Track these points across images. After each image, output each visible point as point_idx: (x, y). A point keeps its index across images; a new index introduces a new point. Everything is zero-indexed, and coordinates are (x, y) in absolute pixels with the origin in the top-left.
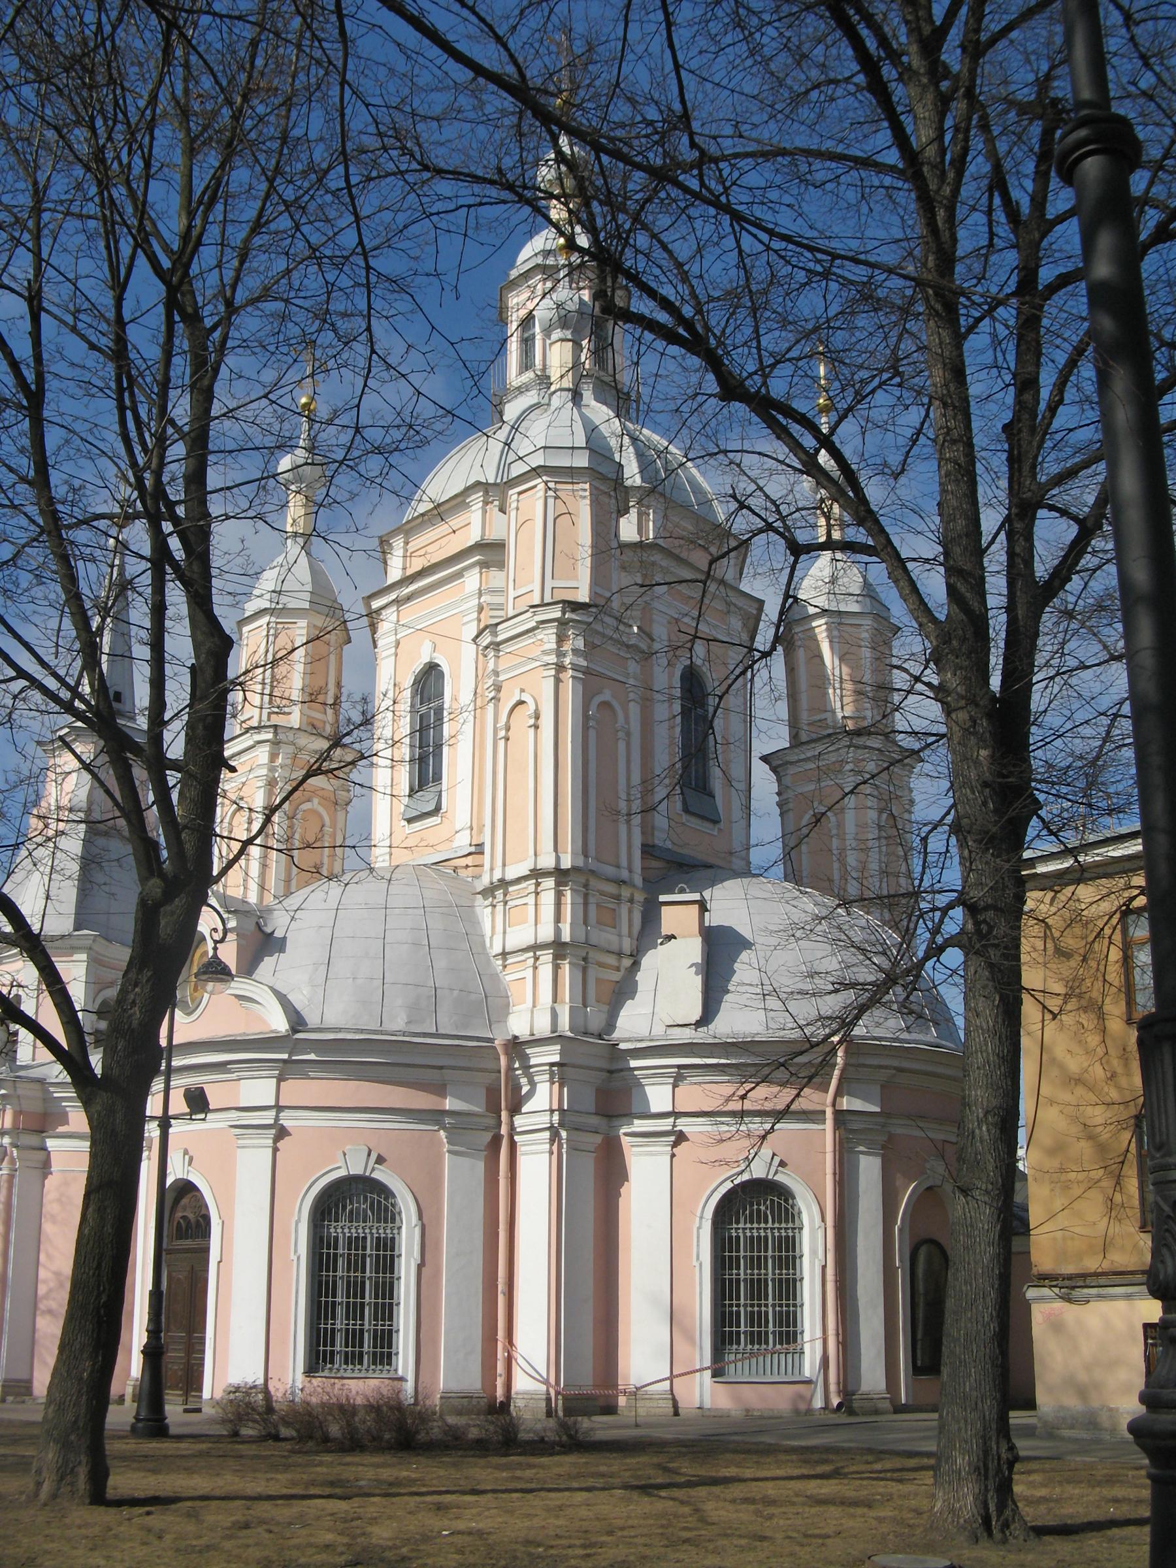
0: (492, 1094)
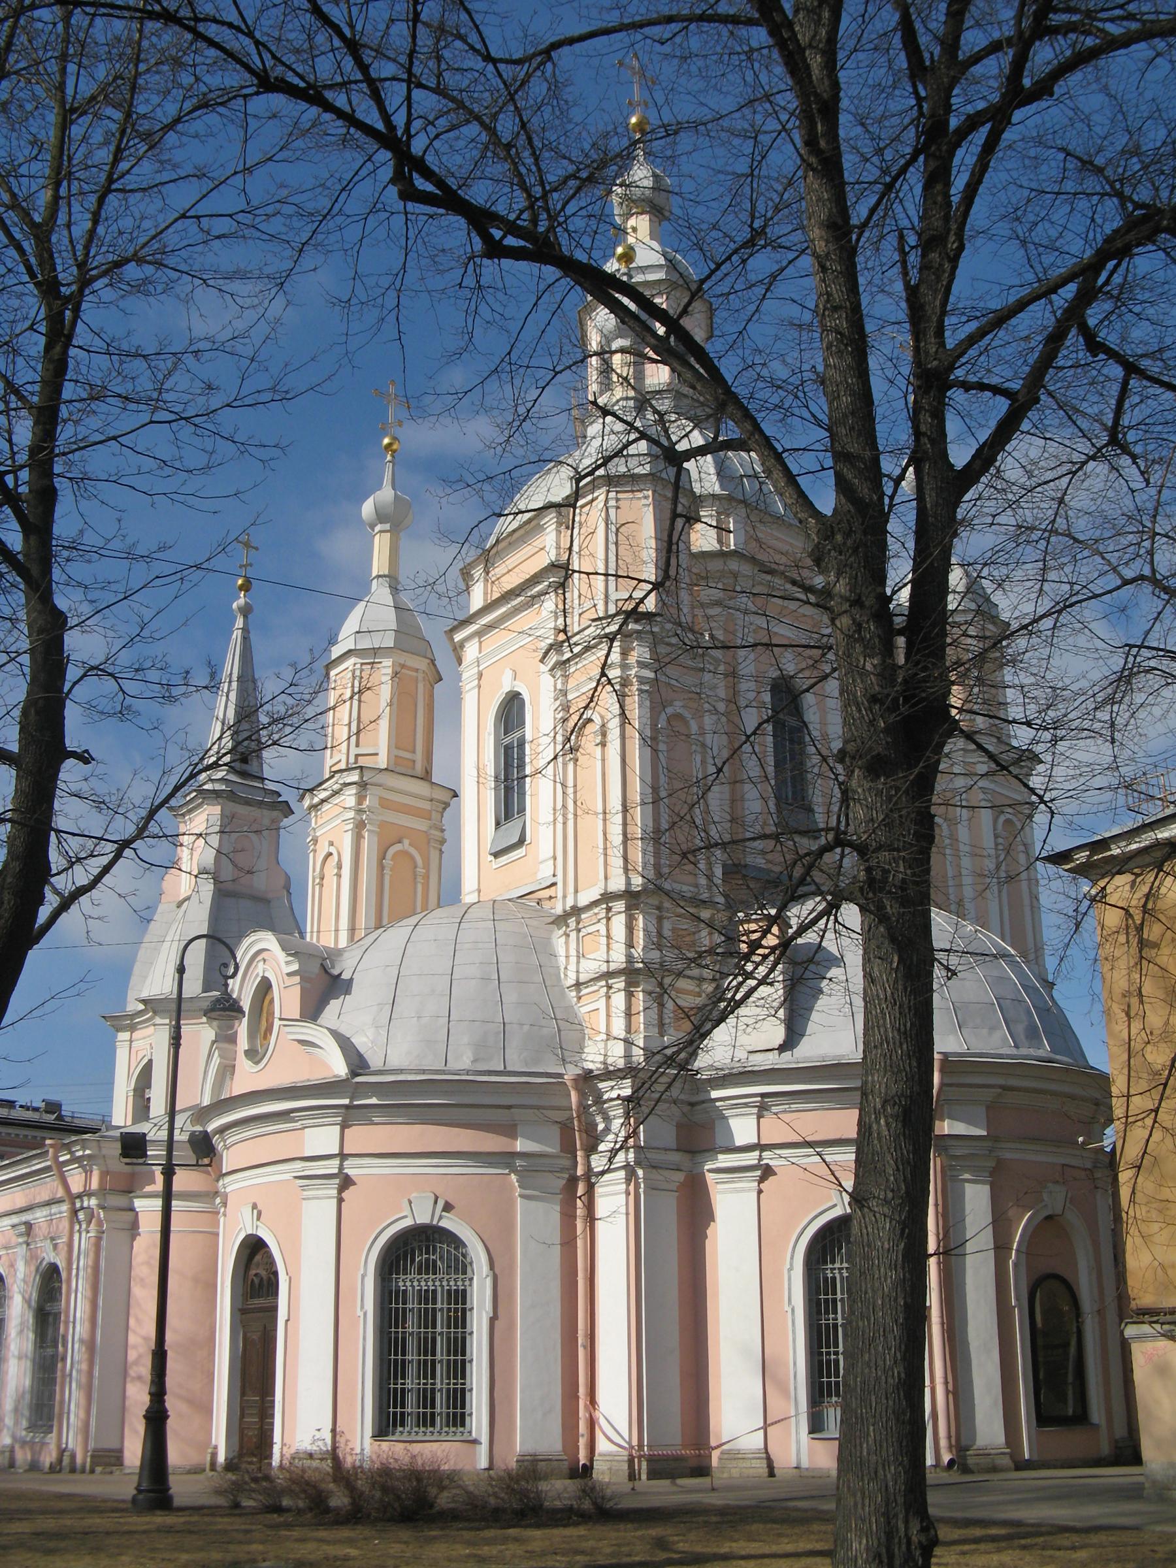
0: (566, 1129)
